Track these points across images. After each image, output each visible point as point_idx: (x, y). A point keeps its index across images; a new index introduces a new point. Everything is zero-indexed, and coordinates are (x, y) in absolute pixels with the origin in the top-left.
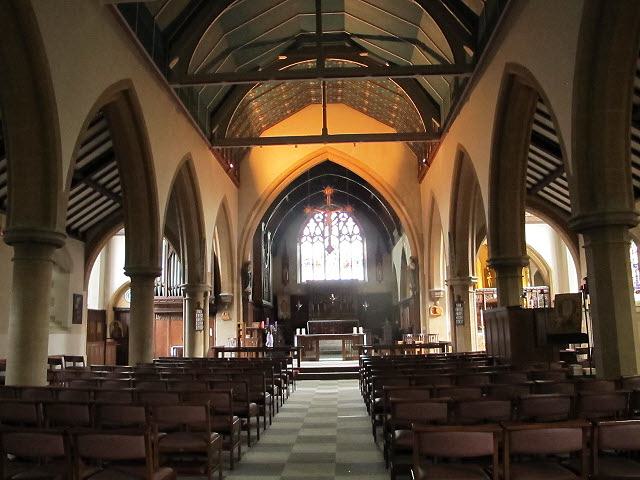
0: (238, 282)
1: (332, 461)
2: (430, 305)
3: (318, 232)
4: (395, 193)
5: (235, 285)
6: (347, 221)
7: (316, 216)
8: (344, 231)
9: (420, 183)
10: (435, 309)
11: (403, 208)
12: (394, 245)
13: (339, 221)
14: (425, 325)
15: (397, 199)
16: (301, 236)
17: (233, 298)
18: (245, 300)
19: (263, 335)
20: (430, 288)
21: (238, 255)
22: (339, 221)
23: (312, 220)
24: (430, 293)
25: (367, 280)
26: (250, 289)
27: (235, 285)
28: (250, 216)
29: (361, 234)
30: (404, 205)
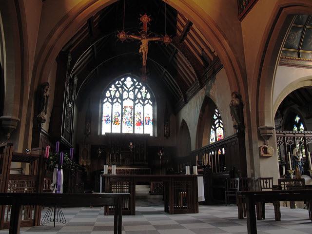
0: (29, 105)
1: (92, 226)
2: (260, 144)
3: (117, 95)
4: (217, 27)
5: (25, 109)
6: (141, 88)
7: (117, 82)
8: (139, 96)
9: (241, 20)
10: (265, 149)
11: (225, 42)
12: (186, 102)
13: (135, 88)
14: (252, 167)
15: (170, 79)
16: (104, 97)
17: (19, 123)
18: (37, 130)
19: (21, 169)
20: (258, 125)
21: (34, 71)
22: (135, 88)
23: (113, 86)
24: (259, 130)
25: (156, 135)
26: (46, 116)
27: (25, 109)
28: (53, 32)
29: (152, 99)
30: (226, 39)
